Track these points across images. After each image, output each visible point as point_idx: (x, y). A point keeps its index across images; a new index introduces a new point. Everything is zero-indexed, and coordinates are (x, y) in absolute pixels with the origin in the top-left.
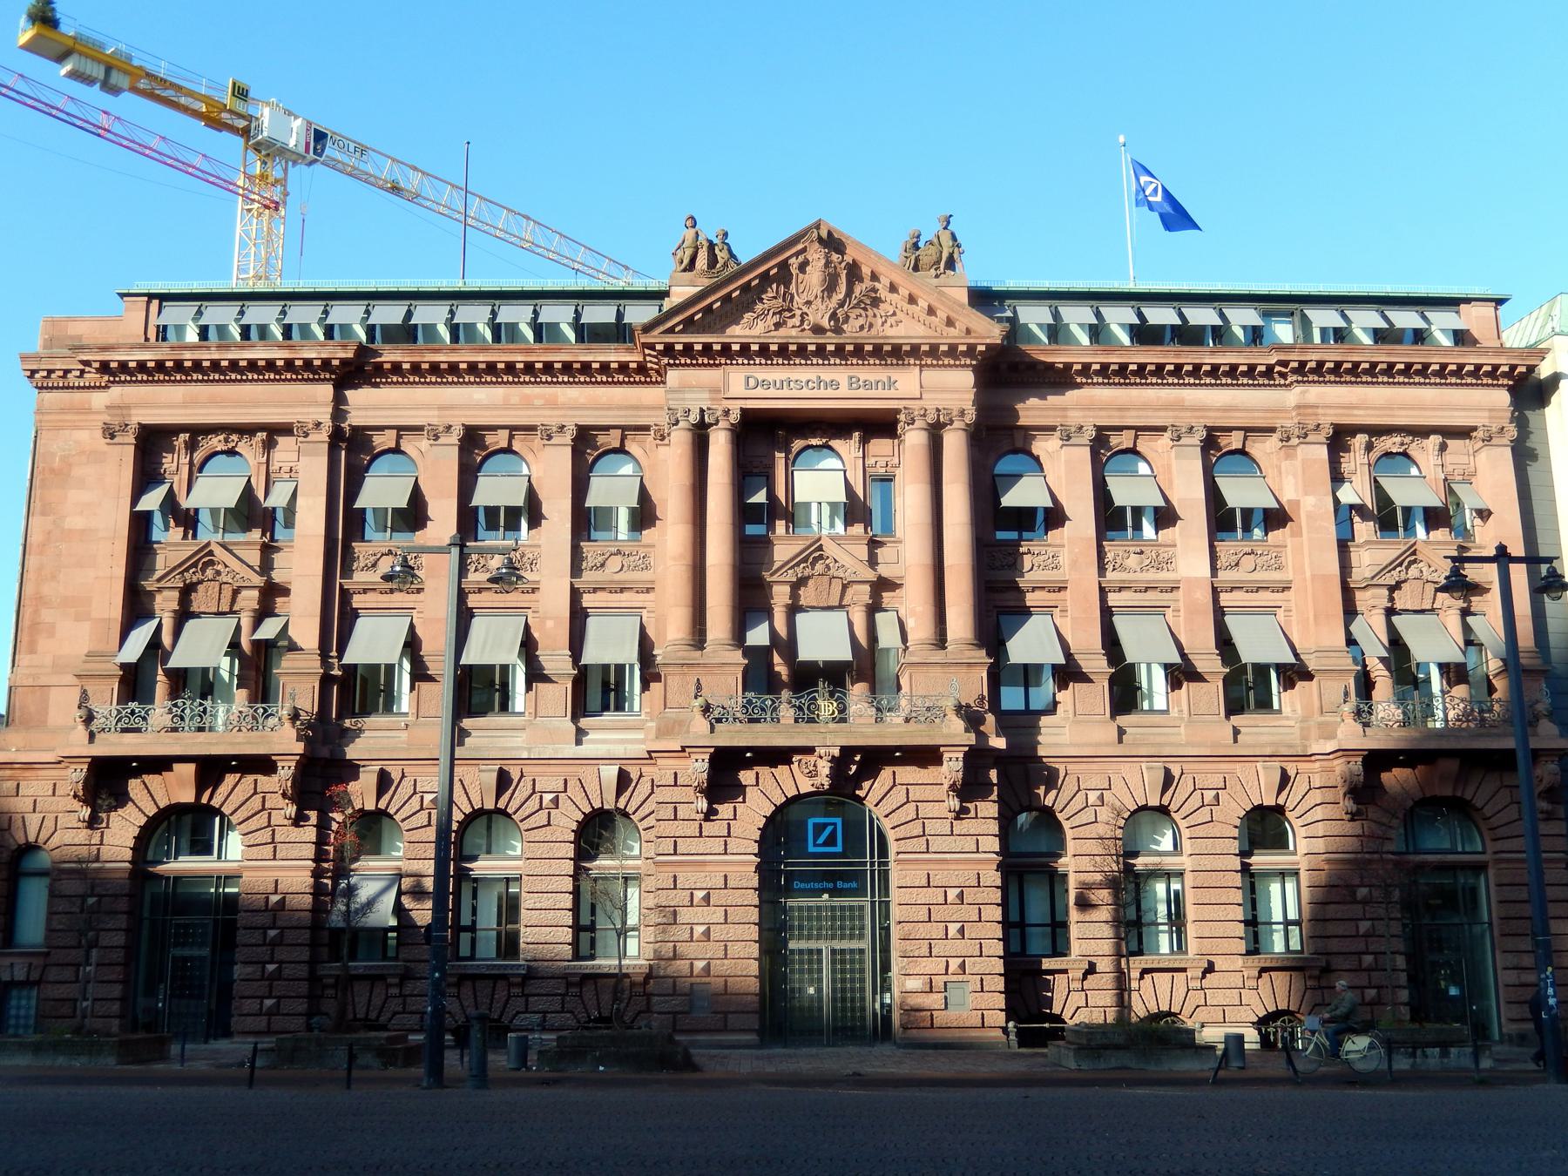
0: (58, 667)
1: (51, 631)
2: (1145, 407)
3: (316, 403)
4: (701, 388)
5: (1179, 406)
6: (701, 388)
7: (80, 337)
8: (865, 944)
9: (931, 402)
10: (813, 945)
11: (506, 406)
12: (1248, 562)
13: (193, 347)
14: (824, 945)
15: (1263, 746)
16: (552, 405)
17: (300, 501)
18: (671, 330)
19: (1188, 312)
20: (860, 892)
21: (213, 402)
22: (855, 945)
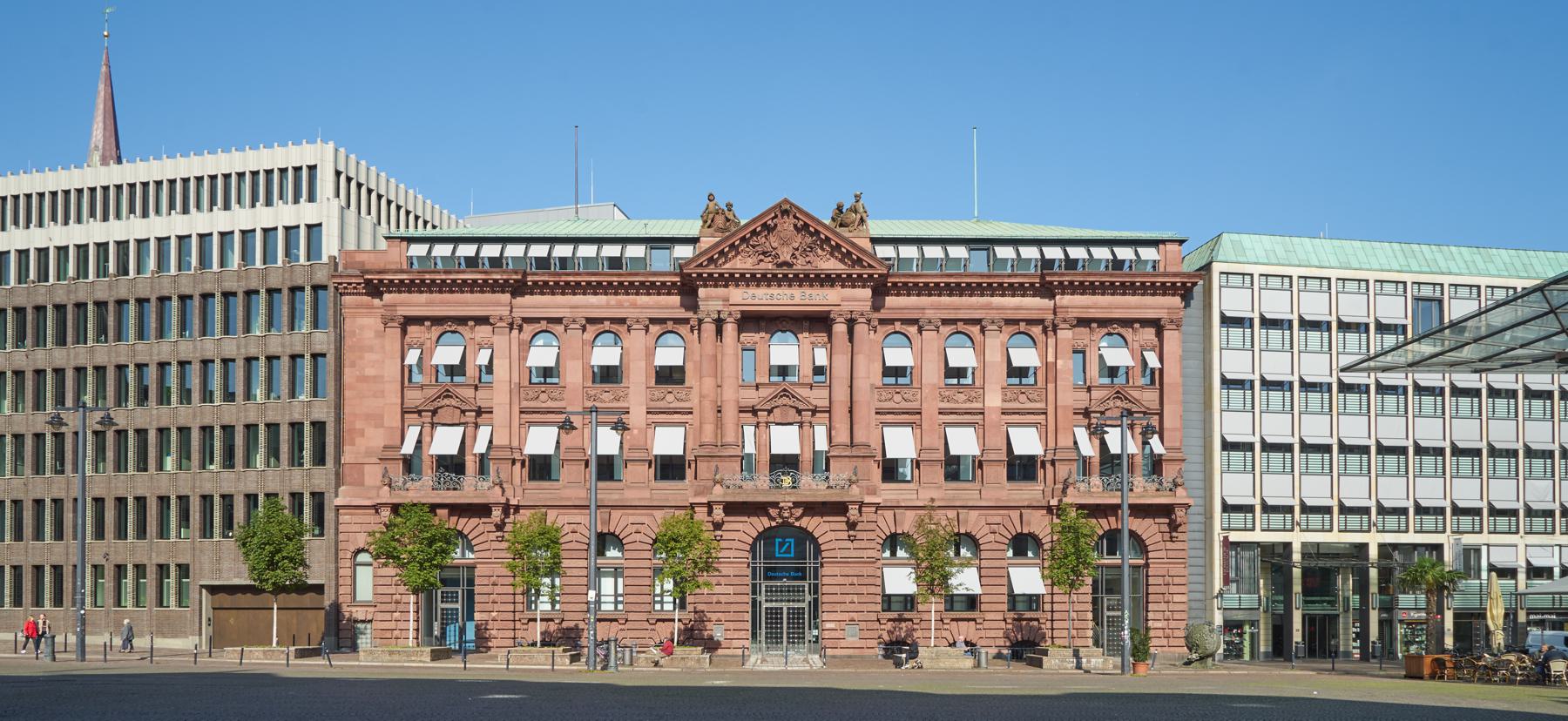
0: (368, 453)
1: (362, 433)
2: (970, 308)
3: (499, 304)
4: (717, 298)
5: (988, 307)
6: (717, 298)
7: (363, 263)
8: (459, 606)
9: (846, 307)
10: (778, 605)
11: (608, 306)
12: (543, 397)
13: (1147, 275)
14: (785, 605)
15: (569, 499)
16: (634, 306)
17: (495, 362)
18: (701, 265)
19: (1070, 250)
20: (804, 578)
21: (443, 303)
22: (769, 605)
